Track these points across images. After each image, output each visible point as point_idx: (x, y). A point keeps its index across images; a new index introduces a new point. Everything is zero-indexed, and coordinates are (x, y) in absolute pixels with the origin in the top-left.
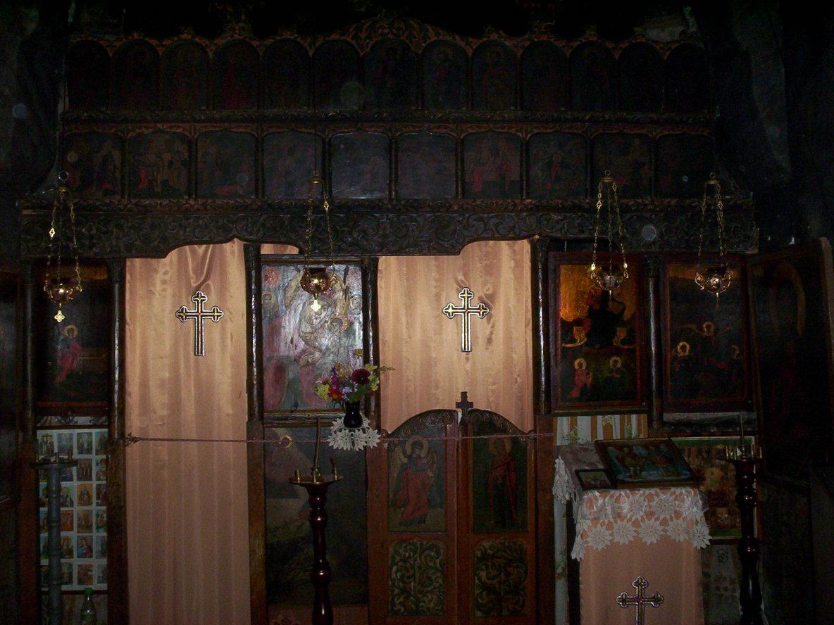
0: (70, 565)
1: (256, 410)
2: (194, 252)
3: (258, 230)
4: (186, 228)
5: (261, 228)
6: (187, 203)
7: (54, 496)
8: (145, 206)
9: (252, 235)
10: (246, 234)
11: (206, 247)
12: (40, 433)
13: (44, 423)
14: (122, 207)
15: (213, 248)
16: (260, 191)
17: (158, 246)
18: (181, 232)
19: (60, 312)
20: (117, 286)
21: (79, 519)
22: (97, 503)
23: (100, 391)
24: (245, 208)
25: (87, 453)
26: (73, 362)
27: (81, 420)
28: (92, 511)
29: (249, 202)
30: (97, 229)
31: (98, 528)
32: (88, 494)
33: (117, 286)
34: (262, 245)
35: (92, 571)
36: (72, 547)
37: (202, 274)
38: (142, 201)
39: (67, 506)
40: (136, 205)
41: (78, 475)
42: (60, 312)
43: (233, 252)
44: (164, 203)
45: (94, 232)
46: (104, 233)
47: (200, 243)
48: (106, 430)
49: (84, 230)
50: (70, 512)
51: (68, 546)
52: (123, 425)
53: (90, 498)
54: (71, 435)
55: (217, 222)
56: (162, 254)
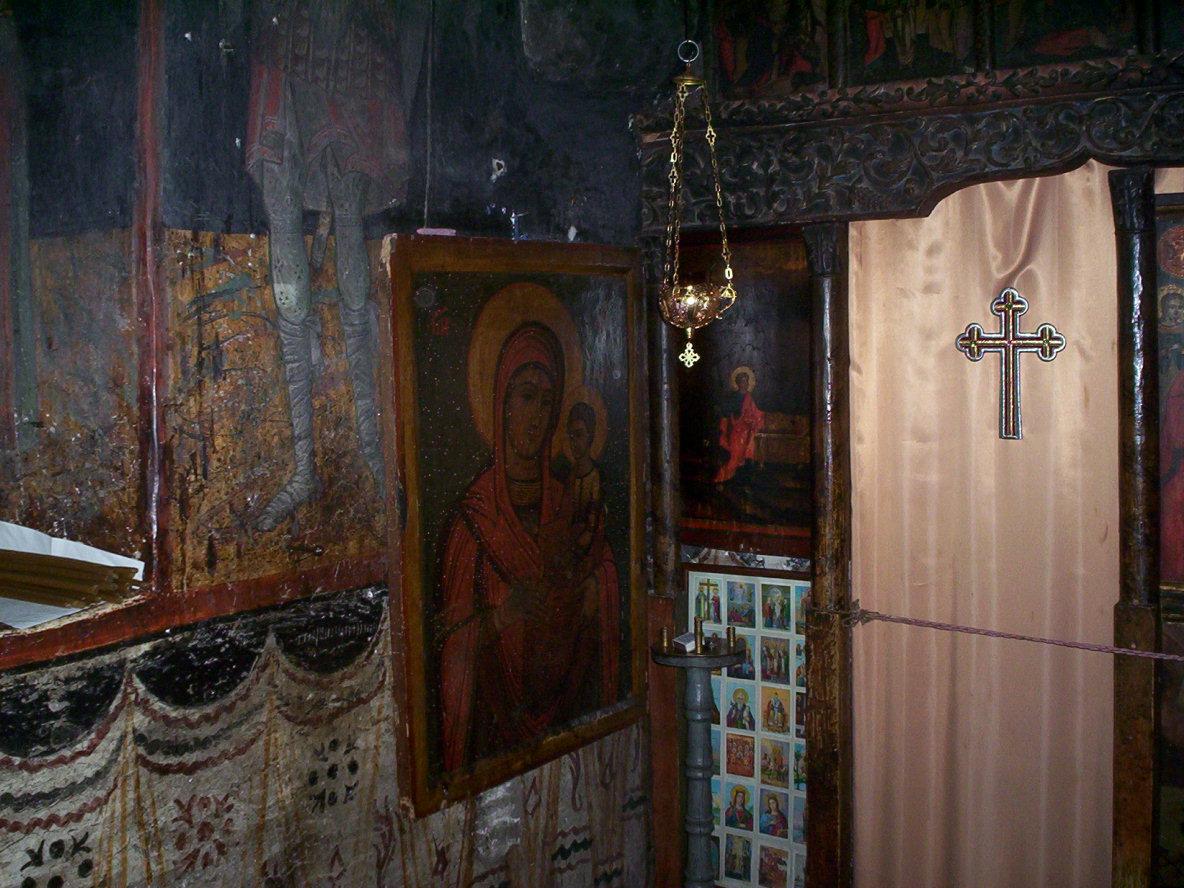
0: (747, 844)
1: (1140, 578)
2: (996, 199)
3: (1145, 135)
4: (969, 143)
5: (1153, 129)
6: (969, 84)
7: (699, 717)
8: (875, 101)
9: (1129, 147)
10: (1114, 145)
11: (1026, 183)
12: (695, 579)
13: (705, 558)
14: (827, 107)
15: (1041, 185)
16: (1150, 34)
17: (907, 191)
18: (960, 154)
19: (689, 346)
20: (827, 284)
21: (765, 757)
22: (798, 731)
23: (796, 499)
24: (1111, 81)
25: (779, 627)
26: (747, 442)
27: (772, 561)
28: (788, 744)
29: (1118, 64)
30: (781, 162)
31: (797, 781)
32: (781, 709)
33: (827, 284)
34: (1157, 170)
35: (785, 863)
36: (752, 808)
37: (1017, 243)
38: (870, 89)
39: (744, 727)
40: (857, 100)
41: (764, 671)
42: (689, 346)
43: (1086, 192)
44: (918, 89)
45: (774, 168)
46: (796, 170)
47: (1009, 176)
48: (808, 584)
49: (755, 167)
50: (749, 740)
51: (743, 805)
52: (844, 582)
53: (785, 718)
54: (752, 586)
55: (1041, 122)
56: (920, 208)
